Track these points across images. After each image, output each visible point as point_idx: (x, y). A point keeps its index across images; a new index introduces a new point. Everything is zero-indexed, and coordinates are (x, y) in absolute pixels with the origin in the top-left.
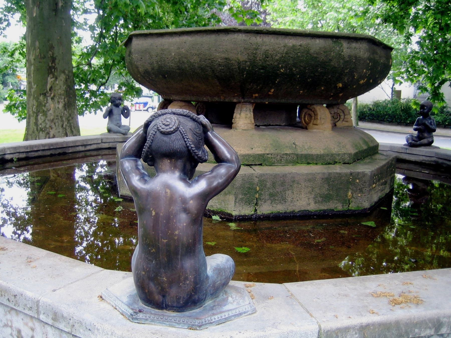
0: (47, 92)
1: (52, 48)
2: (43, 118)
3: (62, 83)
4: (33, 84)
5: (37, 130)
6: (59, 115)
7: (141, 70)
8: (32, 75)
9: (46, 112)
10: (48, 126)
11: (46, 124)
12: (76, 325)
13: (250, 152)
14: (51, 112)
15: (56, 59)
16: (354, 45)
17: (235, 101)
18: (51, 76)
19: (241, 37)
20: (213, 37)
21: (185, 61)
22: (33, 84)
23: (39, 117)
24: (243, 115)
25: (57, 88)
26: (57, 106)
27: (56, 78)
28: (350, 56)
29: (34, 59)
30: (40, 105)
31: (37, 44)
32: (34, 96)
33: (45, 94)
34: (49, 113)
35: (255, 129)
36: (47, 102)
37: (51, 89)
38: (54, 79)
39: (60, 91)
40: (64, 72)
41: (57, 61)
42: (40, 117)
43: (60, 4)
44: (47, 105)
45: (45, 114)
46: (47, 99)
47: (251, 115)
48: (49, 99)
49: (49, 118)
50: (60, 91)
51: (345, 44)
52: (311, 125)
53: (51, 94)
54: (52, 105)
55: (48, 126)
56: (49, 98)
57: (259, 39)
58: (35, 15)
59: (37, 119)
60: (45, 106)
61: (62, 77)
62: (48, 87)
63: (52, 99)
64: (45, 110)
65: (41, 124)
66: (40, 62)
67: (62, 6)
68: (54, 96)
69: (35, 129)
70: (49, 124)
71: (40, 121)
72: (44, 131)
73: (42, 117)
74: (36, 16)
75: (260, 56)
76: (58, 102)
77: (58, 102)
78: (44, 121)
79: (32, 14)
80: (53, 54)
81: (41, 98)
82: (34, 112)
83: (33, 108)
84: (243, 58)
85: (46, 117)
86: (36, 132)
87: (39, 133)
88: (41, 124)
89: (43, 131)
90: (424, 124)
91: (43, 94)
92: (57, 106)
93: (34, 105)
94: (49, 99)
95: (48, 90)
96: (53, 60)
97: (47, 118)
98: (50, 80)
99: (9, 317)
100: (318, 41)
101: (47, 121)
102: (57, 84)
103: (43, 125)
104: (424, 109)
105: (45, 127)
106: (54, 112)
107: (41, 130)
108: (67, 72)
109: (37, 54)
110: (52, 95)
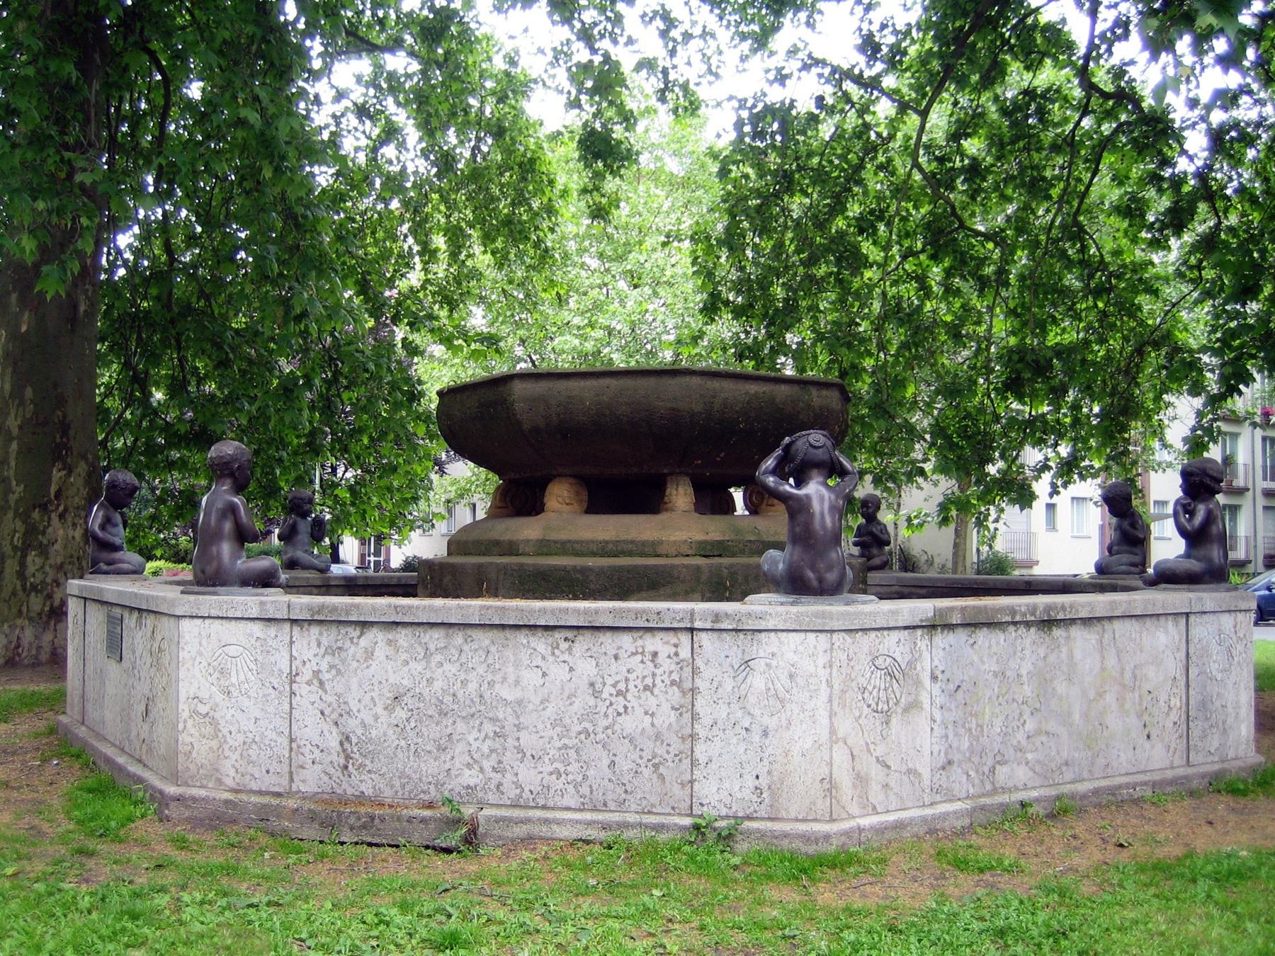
0: (50, 501)
1: (61, 402)
2: (39, 561)
3: (80, 482)
4: (14, 483)
5: (24, 589)
6: (76, 555)
7: (526, 427)
8: (13, 464)
9: (47, 546)
10: (49, 580)
11: (46, 574)
12: (743, 619)
13: (708, 538)
14: (57, 547)
15: (69, 427)
16: (824, 392)
17: (666, 471)
18: (59, 465)
19: (696, 380)
20: (652, 381)
21: (607, 412)
22: (14, 483)
23: (29, 559)
24: (681, 490)
25: (70, 493)
26: (71, 533)
27: (70, 472)
28: (821, 408)
29: (20, 427)
30: (32, 531)
31: (29, 392)
32: (16, 511)
33: (44, 508)
34: (52, 550)
35: (696, 511)
36: (49, 525)
37: (58, 494)
38: (64, 472)
39: (77, 500)
40: (84, 457)
41: (72, 432)
42: (33, 560)
43: (82, 308)
44: (50, 530)
45: (44, 551)
46: (49, 519)
47: (690, 490)
48: (54, 516)
49: (51, 561)
50: (77, 500)
51: (814, 391)
52: (764, 506)
53: (59, 505)
54: (61, 532)
55: (49, 580)
56: (53, 515)
57: (715, 384)
58: (24, 328)
59: (23, 564)
60: (44, 533)
61: (82, 468)
62: (53, 489)
63: (62, 516)
64: (45, 542)
65: (34, 575)
66: (34, 433)
67: (85, 311)
68: (66, 510)
69: (19, 587)
70: (51, 574)
71: (31, 569)
72: (41, 591)
73: (37, 559)
74: (27, 331)
75: (716, 407)
76: (74, 525)
77: (74, 525)
78: (42, 567)
79: (18, 326)
80: (65, 416)
81: (36, 515)
82: (15, 548)
83: (13, 538)
84: (698, 408)
85: (47, 558)
86: (21, 593)
87: (28, 595)
88: (34, 575)
89: (37, 591)
90: (871, 534)
91: (40, 506)
92: (71, 533)
93: (15, 531)
94: (54, 516)
95: (52, 496)
96: (65, 428)
97: (49, 562)
98: (57, 474)
99: (640, 643)
100: (783, 387)
101: (47, 568)
102: (72, 484)
103: (40, 577)
104: (868, 507)
105: (43, 582)
106: (65, 547)
107: (34, 588)
108: (90, 456)
109: (28, 416)
110: (61, 508)
